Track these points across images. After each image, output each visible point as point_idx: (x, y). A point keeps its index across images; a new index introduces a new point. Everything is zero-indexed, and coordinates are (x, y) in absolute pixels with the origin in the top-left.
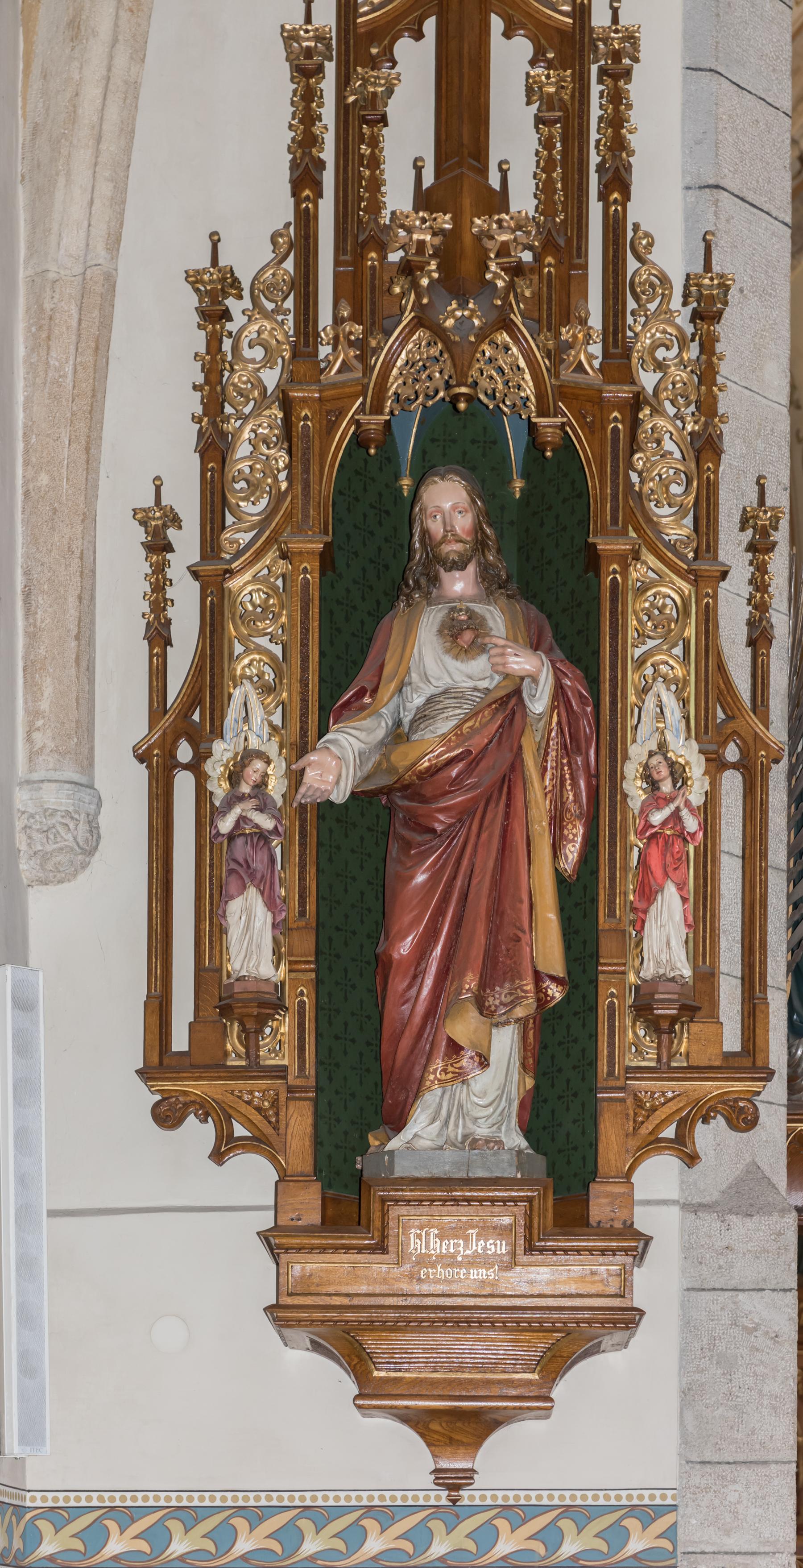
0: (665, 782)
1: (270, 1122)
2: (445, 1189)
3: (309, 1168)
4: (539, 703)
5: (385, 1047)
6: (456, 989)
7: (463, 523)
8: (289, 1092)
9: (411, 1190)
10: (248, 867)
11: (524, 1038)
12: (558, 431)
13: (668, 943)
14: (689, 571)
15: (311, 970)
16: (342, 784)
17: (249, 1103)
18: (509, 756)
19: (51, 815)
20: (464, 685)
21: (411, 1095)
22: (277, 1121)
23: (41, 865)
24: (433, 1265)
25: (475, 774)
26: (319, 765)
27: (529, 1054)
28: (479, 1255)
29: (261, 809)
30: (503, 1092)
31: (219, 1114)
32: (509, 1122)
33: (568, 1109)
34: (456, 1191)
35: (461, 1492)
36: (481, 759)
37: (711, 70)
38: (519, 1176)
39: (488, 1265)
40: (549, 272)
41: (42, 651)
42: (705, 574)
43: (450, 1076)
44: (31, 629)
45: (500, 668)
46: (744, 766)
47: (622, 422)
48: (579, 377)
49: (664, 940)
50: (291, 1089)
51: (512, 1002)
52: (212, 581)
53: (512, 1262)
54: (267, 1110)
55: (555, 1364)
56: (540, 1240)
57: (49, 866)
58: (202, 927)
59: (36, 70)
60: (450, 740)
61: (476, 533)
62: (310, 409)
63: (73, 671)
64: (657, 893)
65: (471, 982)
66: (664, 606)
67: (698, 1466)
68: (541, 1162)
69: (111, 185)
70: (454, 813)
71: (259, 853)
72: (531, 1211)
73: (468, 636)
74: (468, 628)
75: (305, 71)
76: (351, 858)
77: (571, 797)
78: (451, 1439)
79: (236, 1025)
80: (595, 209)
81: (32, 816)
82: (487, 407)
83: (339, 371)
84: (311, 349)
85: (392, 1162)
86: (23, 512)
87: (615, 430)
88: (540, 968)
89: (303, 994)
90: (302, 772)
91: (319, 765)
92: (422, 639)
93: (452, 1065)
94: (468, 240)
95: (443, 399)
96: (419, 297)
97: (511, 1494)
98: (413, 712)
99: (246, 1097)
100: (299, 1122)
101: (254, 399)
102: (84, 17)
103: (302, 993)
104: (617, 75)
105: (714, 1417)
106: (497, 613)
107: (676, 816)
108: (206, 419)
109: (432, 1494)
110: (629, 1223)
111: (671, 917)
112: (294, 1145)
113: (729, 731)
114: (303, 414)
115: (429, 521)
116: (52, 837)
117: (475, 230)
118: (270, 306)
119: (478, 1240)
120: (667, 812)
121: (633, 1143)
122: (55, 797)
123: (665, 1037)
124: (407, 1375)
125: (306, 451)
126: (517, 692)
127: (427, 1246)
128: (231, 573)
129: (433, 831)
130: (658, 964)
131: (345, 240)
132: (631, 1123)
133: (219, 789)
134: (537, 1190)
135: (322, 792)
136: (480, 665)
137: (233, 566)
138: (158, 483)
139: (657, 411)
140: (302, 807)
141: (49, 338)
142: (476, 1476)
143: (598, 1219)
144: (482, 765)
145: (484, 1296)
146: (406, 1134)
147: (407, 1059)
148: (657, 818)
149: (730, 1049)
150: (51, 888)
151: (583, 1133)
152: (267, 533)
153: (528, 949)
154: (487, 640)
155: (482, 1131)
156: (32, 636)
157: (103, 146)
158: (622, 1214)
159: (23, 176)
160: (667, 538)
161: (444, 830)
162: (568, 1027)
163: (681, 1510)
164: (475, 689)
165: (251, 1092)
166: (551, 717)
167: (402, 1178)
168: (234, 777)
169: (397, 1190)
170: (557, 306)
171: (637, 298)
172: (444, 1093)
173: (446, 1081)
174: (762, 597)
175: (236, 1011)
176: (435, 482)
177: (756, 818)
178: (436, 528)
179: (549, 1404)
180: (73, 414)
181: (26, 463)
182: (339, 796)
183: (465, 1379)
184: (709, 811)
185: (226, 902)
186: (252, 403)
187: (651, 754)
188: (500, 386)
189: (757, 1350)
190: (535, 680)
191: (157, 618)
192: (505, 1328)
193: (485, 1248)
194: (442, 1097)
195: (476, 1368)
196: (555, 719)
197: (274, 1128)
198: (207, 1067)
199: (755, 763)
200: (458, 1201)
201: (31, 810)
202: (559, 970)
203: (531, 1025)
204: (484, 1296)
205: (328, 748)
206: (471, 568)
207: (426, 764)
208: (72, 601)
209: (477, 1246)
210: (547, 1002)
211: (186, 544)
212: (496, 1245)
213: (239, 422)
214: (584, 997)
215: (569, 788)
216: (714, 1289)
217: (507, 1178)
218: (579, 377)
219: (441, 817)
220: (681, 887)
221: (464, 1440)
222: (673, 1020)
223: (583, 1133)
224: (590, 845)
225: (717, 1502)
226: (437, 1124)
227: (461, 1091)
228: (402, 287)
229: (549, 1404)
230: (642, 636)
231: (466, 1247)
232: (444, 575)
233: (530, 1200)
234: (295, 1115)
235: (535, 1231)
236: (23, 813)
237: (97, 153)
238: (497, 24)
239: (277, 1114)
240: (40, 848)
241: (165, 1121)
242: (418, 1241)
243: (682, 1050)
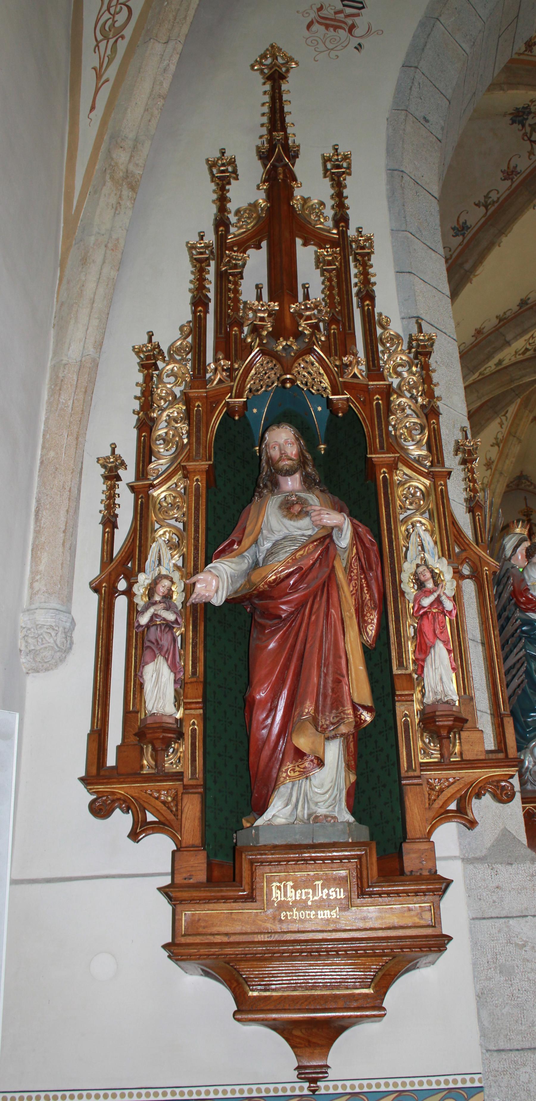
0: (429, 582)
1: (172, 811)
2: (298, 852)
3: (198, 841)
4: (344, 540)
5: (251, 758)
6: (298, 714)
7: (292, 450)
8: (184, 789)
9: (272, 854)
10: (158, 644)
11: (347, 747)
12: (345, 403)
13: (441, 679)
14: (428, 473)
15: (200, 708)
16: (220, 593)
17: (157, 798)
18: (326, 570)
19: (40, 627)
20: (296, 533)
21: (271, 789)
22: (177, 810)
23: (34, 659)
24: (290, 909)
25: (305, 581)
26: (204, 581)
27: (351, 758)
28: (324, 900)
29: (167, 609)
30: (335, 784)
31: (133, 806)
32: (340, 805)
33: (380, 795)
34: (306, 853)
35: (319, 1083)
36: (308, 574)
37: (409, 272)
38: (350, 841)
39: (331, 908)
40: (334, 332)
41: (43, 539)
42: (438, 476)
43: (297, 773)
44: (38, 528)
45: (318, 523)
46: (475, 577)
47: (381, 400)
48: (355, 381)
49: (438, 678)
50: (185, 787)
51: (338, 721)
52: (141, 491)
53: (348, 905)
54: (170, 802)
55: (384, 982)
56: (369, 887)
57: (38, 659)
58: (129, 686)
59: (65, 281)
60: (288, 563)
61: (300, 457)
62: (200, 401)
63: (61, 550)
64: (431, 647)
65: (309, 708)
66: (416, 492)
67: (495, 1054)
68: (364, 833)
69: (98, 321)
70: (293, 605)
71: (166, 636)
72: (361, 865)
73: (297, 508)
74: (297, 503)
75: (200, 266)
76: (229, 644)
77: (368, 598)
78: (309, 1042)
79: (150, 747)
80: (357, 314)
81: (29, 629)
82: (303, 389)
83: (218, 384)
84: (202, 375)
85: (257, 835)
86: (39, 472)
87: (378, 404)
88: (356, 700)
89: (194, 725)
90: (194, 584)
91: (204, 581)
92: (269, 512)
93: (298, 766)
94: (288, 321)
95: (277, 386)
96: (261, 340)
97: (356, 1083)
98: (265, 553)
99: (156, 795)
100: (191, 808)
101: (169, 401)
102: (89, 255)
103: (194, 724)
104: (364, 260)
105: (503, 1014)
106: (314, 498)
107: (438, 601)
108: (142, 413)
109: (297, 1085)
110: (433, 871)
111: (441, 663)
112: (187, 825)
113: (464, 557)
114: (197, 404)
115: (271, 451)
116: (40, 640)
117: (292, 311)
118: (178, 358)
119: (322, 889)
120: (432, 598)
121: (431, 814)
122: (43, 618)
123: (444, 741)
124: (274, 994)
125: (199, 422)
126: (330, 536)
127: (285, 895)
128: (152, 486)
129: (280, 617)
130: (436, 693)
131: (221, 329)
132: (427, 800)
133: (140, 601)
134: (364, 850)
135: (206, 597)
136: (305, 522)
137: (155, 482)
138: (113, 446)
139: (400, 396)
140: (194, 606)
141: (60, 389)
142: (329, 1071)
143: (410, 869)
144: (310, 576)
145: (330, 931)
146: (267, 816)
147: (267, 766)
148: (426, 602)
149: (489, 749)
150: (41, 674)
151: (392, 811)
152: (176, 464)
153: (347, 688)
154: (309, 508)
155: (322, 811)
156: (38, 532)
157: (95, 305)
158: (429, 865)
159: (54, 325)
160: (412, 457)
161: (287, 616)
162: (376, 742)
163: (486, 1090)
164: (303, 535)
165: (158, 791)
166: (352, 550)
167: (265, 846)
168: (151, 590)
169: (261, 854)
170: (341, 344)
171: (383, 345)
172: (293, 786)
173: (295, 777)
174: (474, 486)
175: (148, 736)
176: (274, 430)
177: (487, 606)
178: (275, 453)
179: (383, 1013)
180: (71, 422)
181: (43, 448)
182: (218, 600)
183: (318, 995)
184: (457, 599)
185: (143, 667)
186: (167, 403)
187: (418, 566)
188: (310, 380)
189: (528, 961)
190: (340, 529)
191: (109, 513)
192: (346, 956)
193: (328, 895)
194: (292, 788)
195: (325, 987)
196: (355, 551)
197: (174, 815)
198: (128, 775)
199: (482, 574)
200: (307, 860)
201: (29, 626)
202: (369, 703)
203: (351, 739)
204: (330, 931)
205: (210, 571)
206: (297, 476)
207: (274, 577)
208: (63, 513)
209: (322, 893)
210: (361, 724)
211: (128, 475)
212: (336, 892)
213: (160, 412)
214: (385, 721)
215: (366, 592)
216: (492, 918)
217: (341, 842)
218: (355, 381)
219: (284, 607)
220: (446, 643)
221: (320, 1042)
222: (450, 729)
223: (392, 811)
224: (383, 627)
225: (513, 1082)
226: (290, 807)
227: (305, 784)
228: (252, 339)
229: (383, 1013)
230: (404, 508)
231: (314, 894)
232: (281, 479)
233: (359, 857)
234: (188, 804)
235: (365, 880)
236: (24, 628)
237: (92, 308)
238: (299, 241)
239: (177, 805)
240: (33, 648)
241: (99, 813)
242: (278, 891)
243: (456, 751)
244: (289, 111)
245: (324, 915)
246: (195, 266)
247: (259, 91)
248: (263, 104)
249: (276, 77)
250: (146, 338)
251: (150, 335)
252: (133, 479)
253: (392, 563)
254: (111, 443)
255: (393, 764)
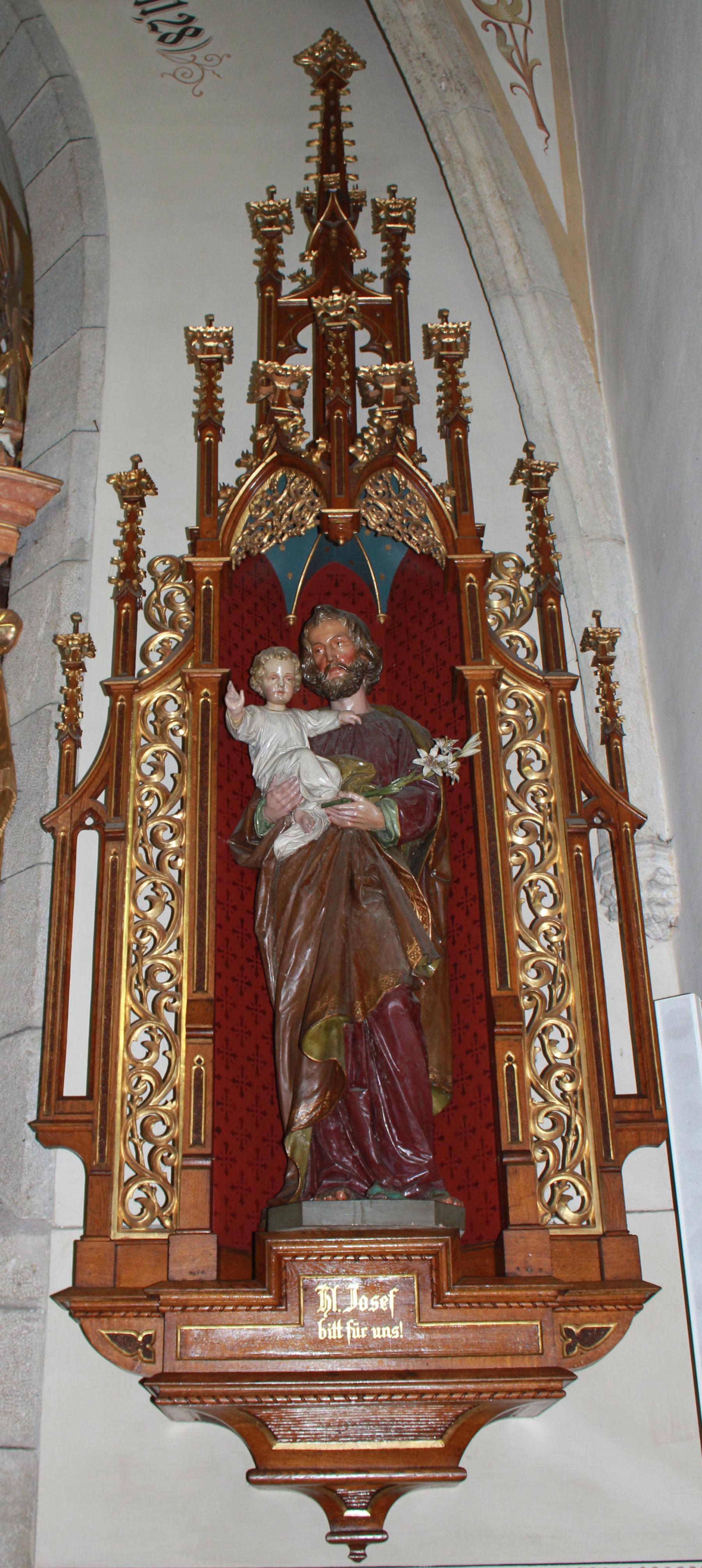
138: (137, 459)
211: (99, 667)
244: (349, 120)
245: (381, 1333)
246: (202, 370)
247: (305, 99)
248: (311, 126)
249: (330, 76)
250: (129, 466)
251: (136, 460)
252: (108, 674)
253: (498, 908)
254: (132, 454)
255: (474, 899)
